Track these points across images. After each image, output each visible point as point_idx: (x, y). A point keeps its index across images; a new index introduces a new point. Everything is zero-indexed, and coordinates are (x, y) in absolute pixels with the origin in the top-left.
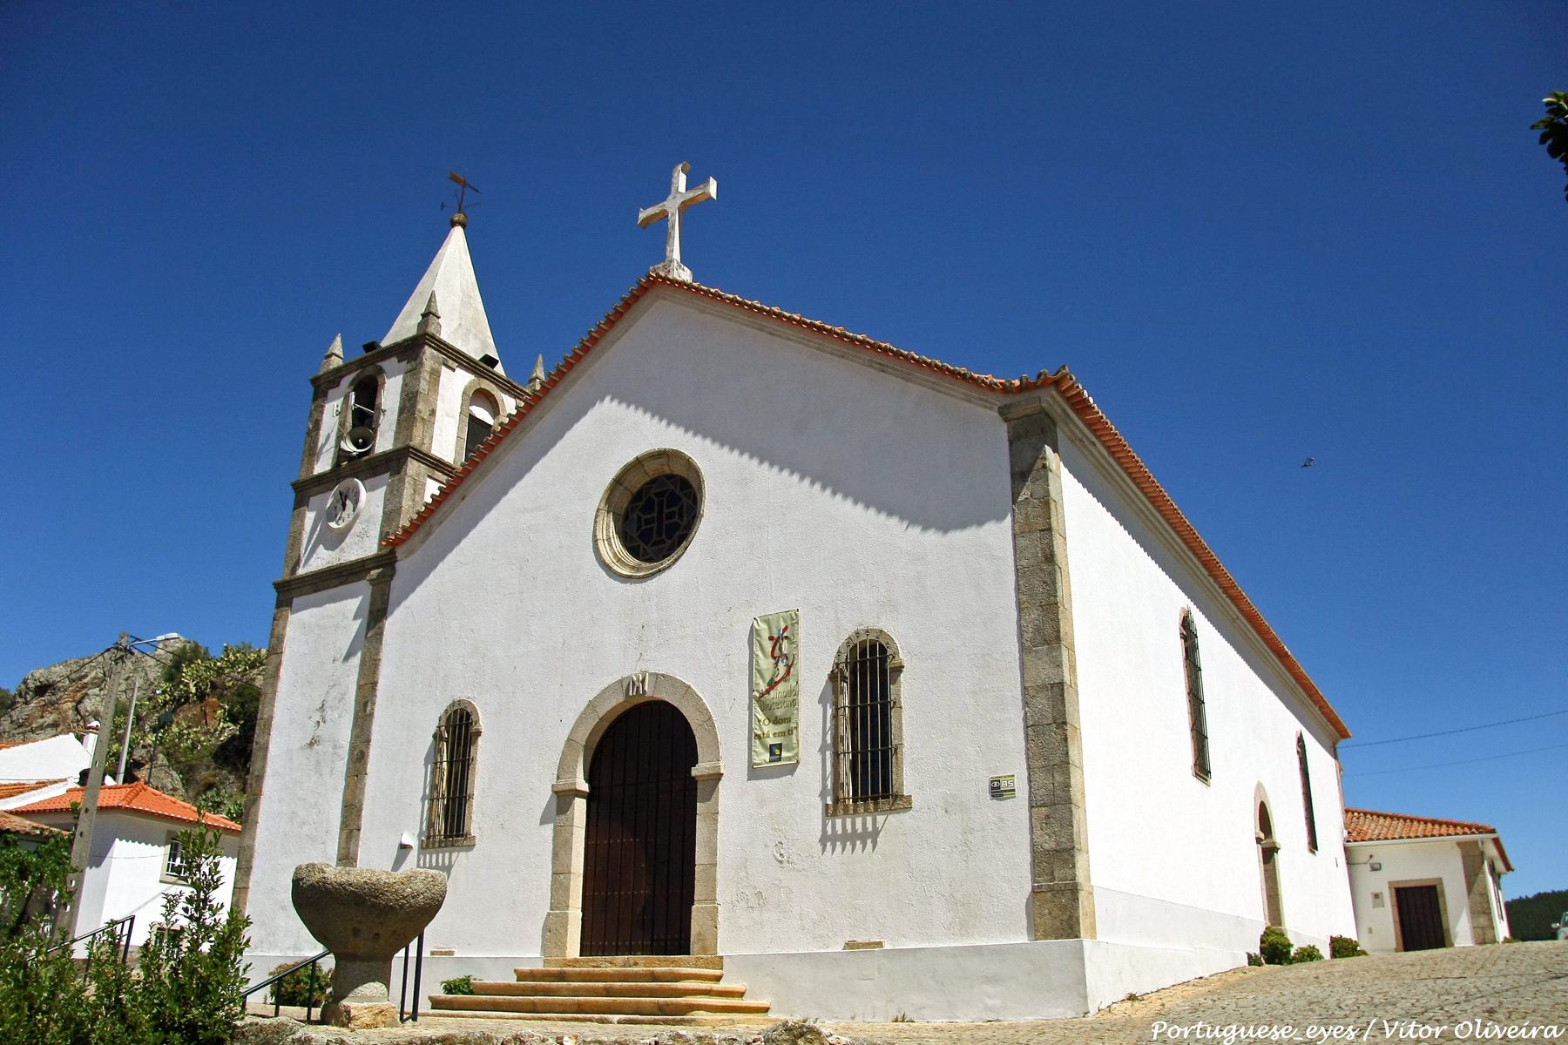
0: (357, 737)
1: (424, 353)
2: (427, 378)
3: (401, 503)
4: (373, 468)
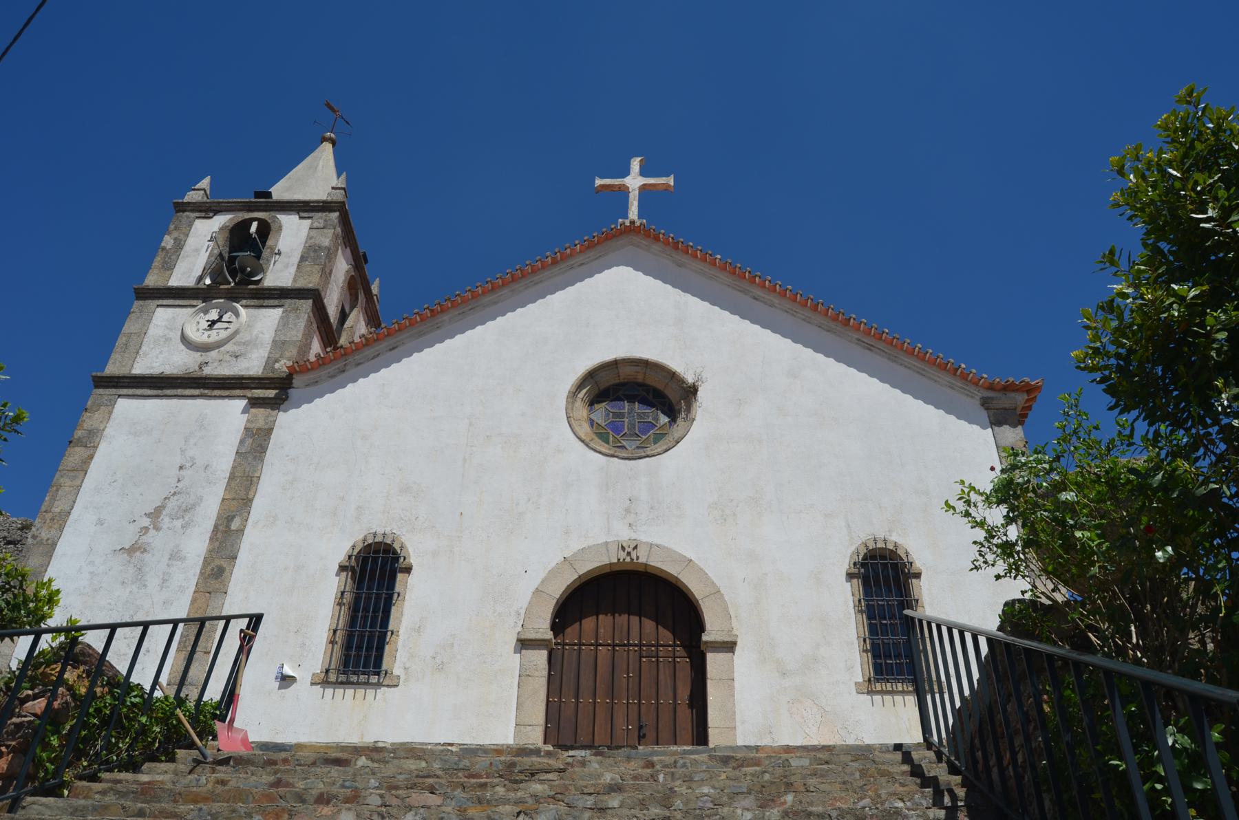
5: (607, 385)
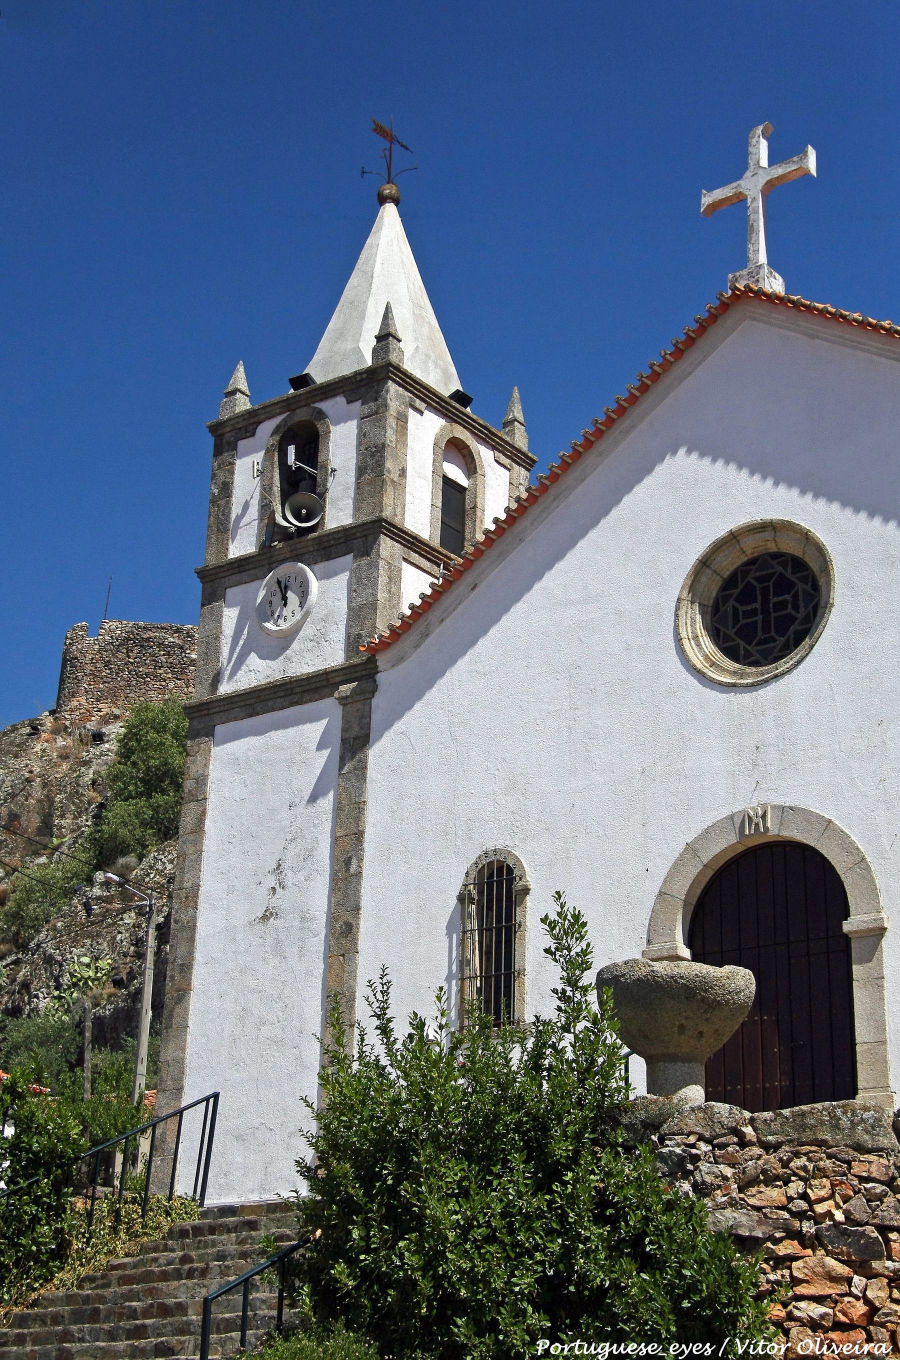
0: (338, 904)
1: (387, 391)
2: (394, 425)
3: (375, 595)
4: (325, 548)
5: (732, 569)
